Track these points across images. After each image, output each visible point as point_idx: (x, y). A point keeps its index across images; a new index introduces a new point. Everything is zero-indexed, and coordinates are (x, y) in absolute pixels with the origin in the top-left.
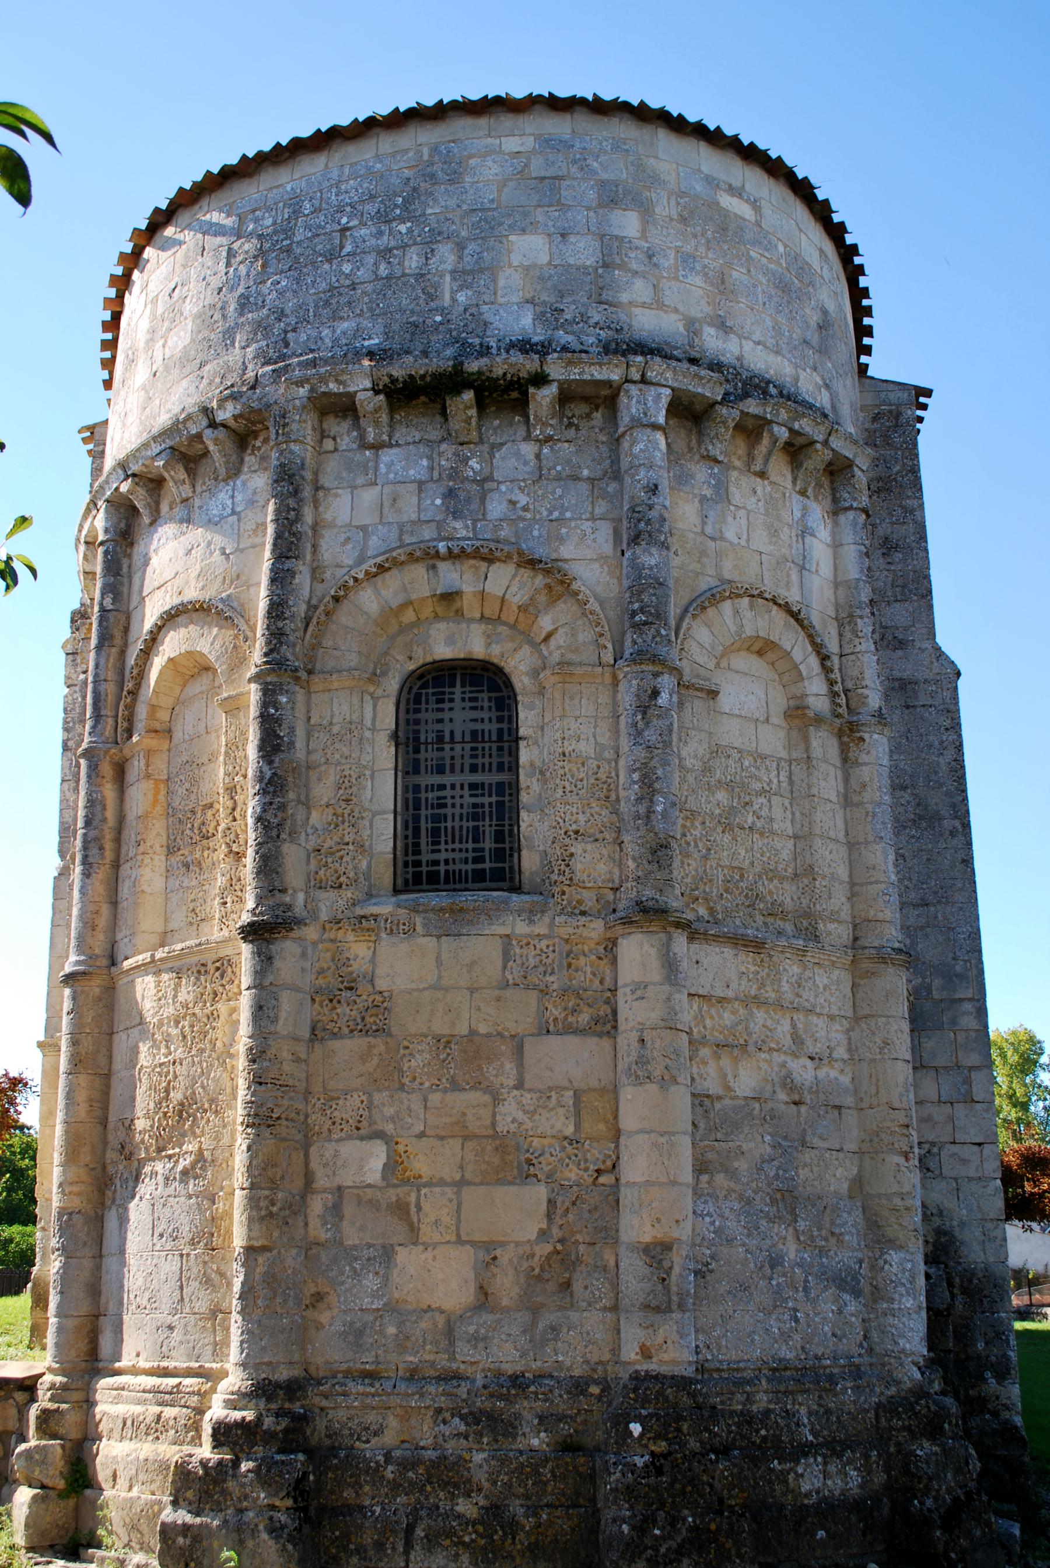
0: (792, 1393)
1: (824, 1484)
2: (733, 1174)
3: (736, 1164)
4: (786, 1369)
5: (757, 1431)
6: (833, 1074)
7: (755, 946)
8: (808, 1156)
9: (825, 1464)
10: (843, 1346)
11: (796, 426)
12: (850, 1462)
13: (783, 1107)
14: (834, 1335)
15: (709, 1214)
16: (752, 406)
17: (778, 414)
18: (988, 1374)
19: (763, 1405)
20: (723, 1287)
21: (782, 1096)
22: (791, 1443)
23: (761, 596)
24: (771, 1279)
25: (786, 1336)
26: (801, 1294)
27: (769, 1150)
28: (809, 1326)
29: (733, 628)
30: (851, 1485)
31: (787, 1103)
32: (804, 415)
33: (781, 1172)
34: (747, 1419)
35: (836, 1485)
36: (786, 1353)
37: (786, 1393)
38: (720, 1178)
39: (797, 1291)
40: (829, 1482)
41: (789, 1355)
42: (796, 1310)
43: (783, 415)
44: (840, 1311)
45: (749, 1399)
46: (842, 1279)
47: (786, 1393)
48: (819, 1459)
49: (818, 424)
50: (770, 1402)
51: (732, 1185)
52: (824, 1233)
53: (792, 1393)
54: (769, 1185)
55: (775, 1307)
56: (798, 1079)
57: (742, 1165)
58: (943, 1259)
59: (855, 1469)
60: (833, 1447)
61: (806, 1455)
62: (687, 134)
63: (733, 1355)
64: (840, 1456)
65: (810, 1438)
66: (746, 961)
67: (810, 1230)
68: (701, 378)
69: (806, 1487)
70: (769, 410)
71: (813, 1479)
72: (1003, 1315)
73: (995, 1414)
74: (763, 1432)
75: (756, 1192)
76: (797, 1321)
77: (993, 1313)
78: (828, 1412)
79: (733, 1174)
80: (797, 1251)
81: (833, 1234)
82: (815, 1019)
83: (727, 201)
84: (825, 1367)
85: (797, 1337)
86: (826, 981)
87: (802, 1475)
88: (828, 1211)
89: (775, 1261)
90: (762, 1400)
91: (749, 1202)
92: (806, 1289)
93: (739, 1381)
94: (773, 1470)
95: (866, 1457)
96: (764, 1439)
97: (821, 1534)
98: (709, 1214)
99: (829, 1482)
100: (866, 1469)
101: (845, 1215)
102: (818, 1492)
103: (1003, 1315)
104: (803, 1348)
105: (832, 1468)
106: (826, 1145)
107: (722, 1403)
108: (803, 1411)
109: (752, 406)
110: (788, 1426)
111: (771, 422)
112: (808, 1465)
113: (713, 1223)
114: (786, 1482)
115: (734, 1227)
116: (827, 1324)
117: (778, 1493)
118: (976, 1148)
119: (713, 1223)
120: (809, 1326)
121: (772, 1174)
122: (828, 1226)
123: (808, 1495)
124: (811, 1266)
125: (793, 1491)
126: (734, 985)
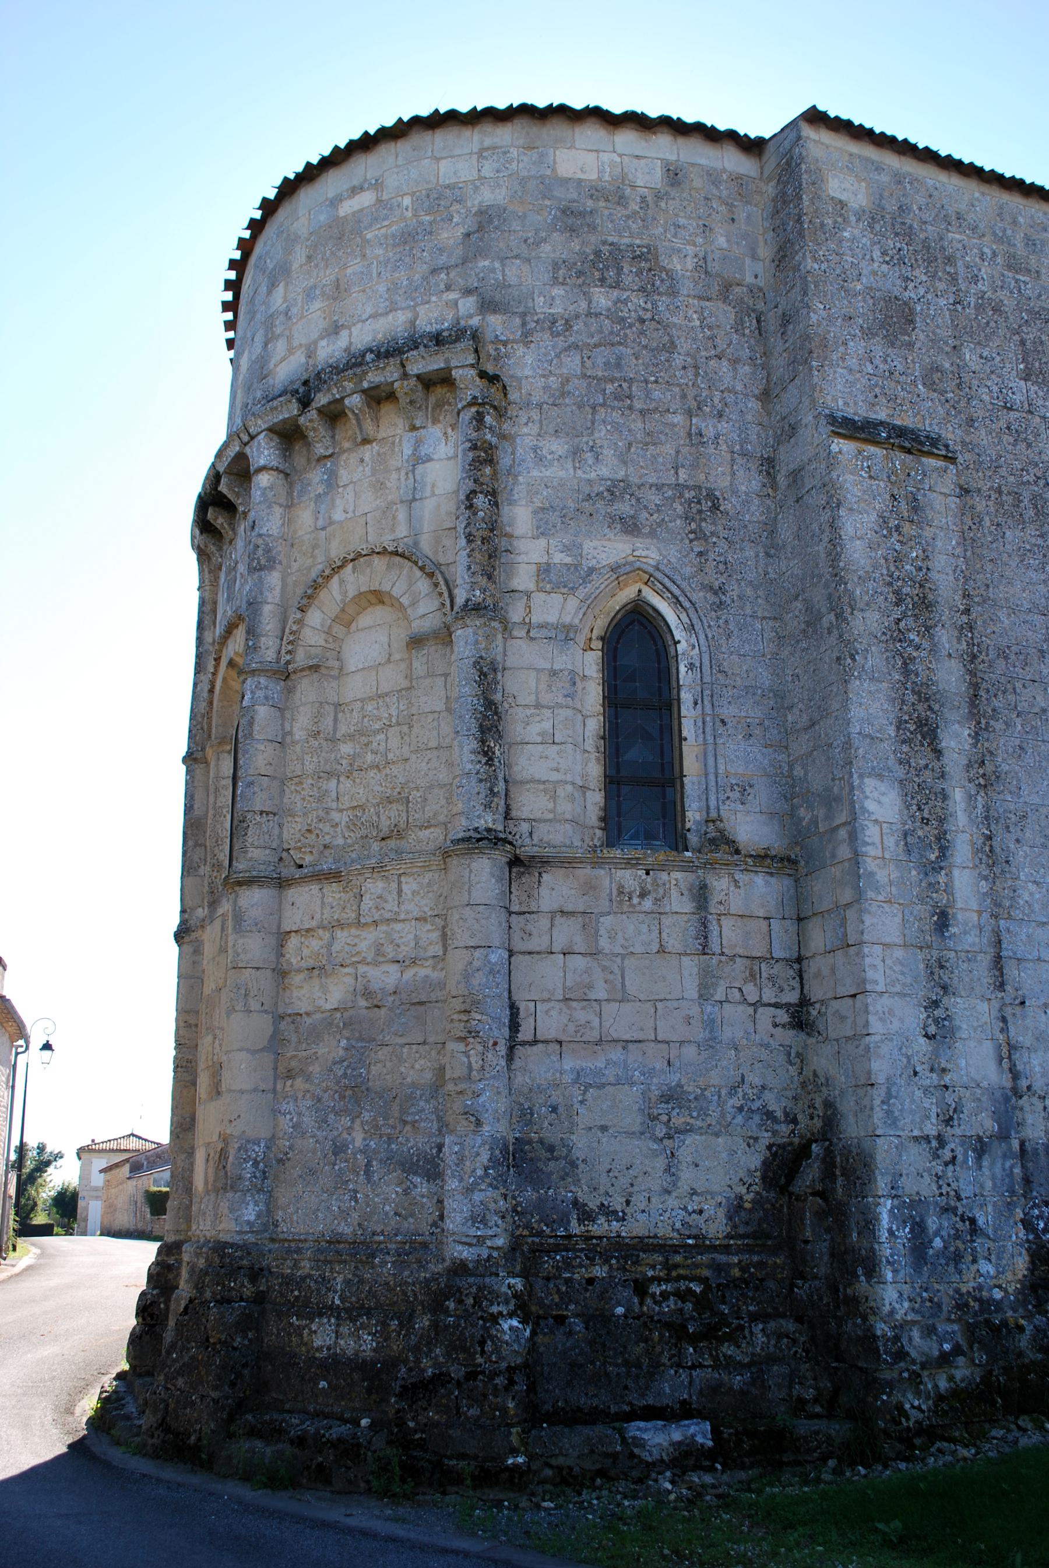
0: (330, 1262)
1: (336, 1343)
2: (308, 1078)
3: (311, 1069)
4: (339, 1242)
5: (292, 1291)
8: (382, 1053)
9: (338, 1325)
10: (409, 1224)
11: (365, 385)
12: (363, 1327)
13: (365, 1011)
14: (396, 1214)
15: (290, 1113)
16: (322, 399)
17: (344, 388)
19: (307, 1271)
20: (297, 1172)
21: (363, 1003)
22: (317, 1304)
23: (359, 555)
24: (334, 1164)
25: (345, 1214)
26: (362, 1178)
27: (341, 1052)
28: (368, 1205)
30: (364, 1347)
31: (367, 1008)
32: (365, 373)
33: (349, 1071)
34: (288, 1281)
35: (348, 1345)
36: (345, 1229)
37: (326, 1262)
38: (299, 1082)
39: (358, 1174)
40: (342, 1342)
41: (348, 1230)
42: (356, 1191)
43: (349, 386)
44: (406, 1192)
45: (296, 1266)
46: (412, 1163)
47: (326, 1262)
48: (333, 1320)
49: (384, 368)
50: (312, 1268)
52: (391, 1122)
53: (330, 1262)
54: (338, 1083)
55: (336, 1188)
56: (375, 986)
57: (315, 1069)
58: (829, 1135)
59: (369, 1334)
60: (352, 1313)
61: (321, 1315)
62: (319, 175)
63: (301, 1228)
64: (353, 1320)
65: (337, 1302)
66: (333, 892)
67: (375, 1119)
68: (276, 408)
69: (318, 1342)
70: (335, 391)
71: (322, 1336)
72: (871, 1200)
73: (865, 1319)
74: (296, 1293)
76: (357, 1201)
77: (863, 1197)
78: (361, 1281)
79: (308, 1078)
80: (364, 1139)
81: (405, 1123)
82: (398, 926)
84: (380, 1243)
85: (355, 1215)
86: (415, 887)
87: (315, 1332)
88: (398, 1101)
89: (339, 1149)
90: (306, 1266)
91: (319, 1100)
92: (368, 1173)
93: (292, 1248)
94: (292, 1324)
95: (385, 1324)
96: (297, 1297)
97: (323, 1384)
98: (290, 1113)
99: (342, 1342)
100: (384, 1335)
101: (422, 1103)
102: (329, 1349)
103: (871, 1200)
104: (359, 1225)
105: (344, 1330)
106: (403, 1040)
107: (277, 1266)
108: (340, 1279)
109: (322, 399)
110: (318, 1290)
111: (343, 398)
112: (321, 1325)
113: (291, 1120)
114: (301, 1335)
115: (309, 1121)
116: (384, 1203)
117: (294, 1344)
118: (850, 1001)
119: (291, 1120)
120: (368, 1205)
121: (340, 1073)
122: (397, 1115)
123: (319, 1349)
124: (376, 1152)
125: (306, 1344)
126: (318, 916)
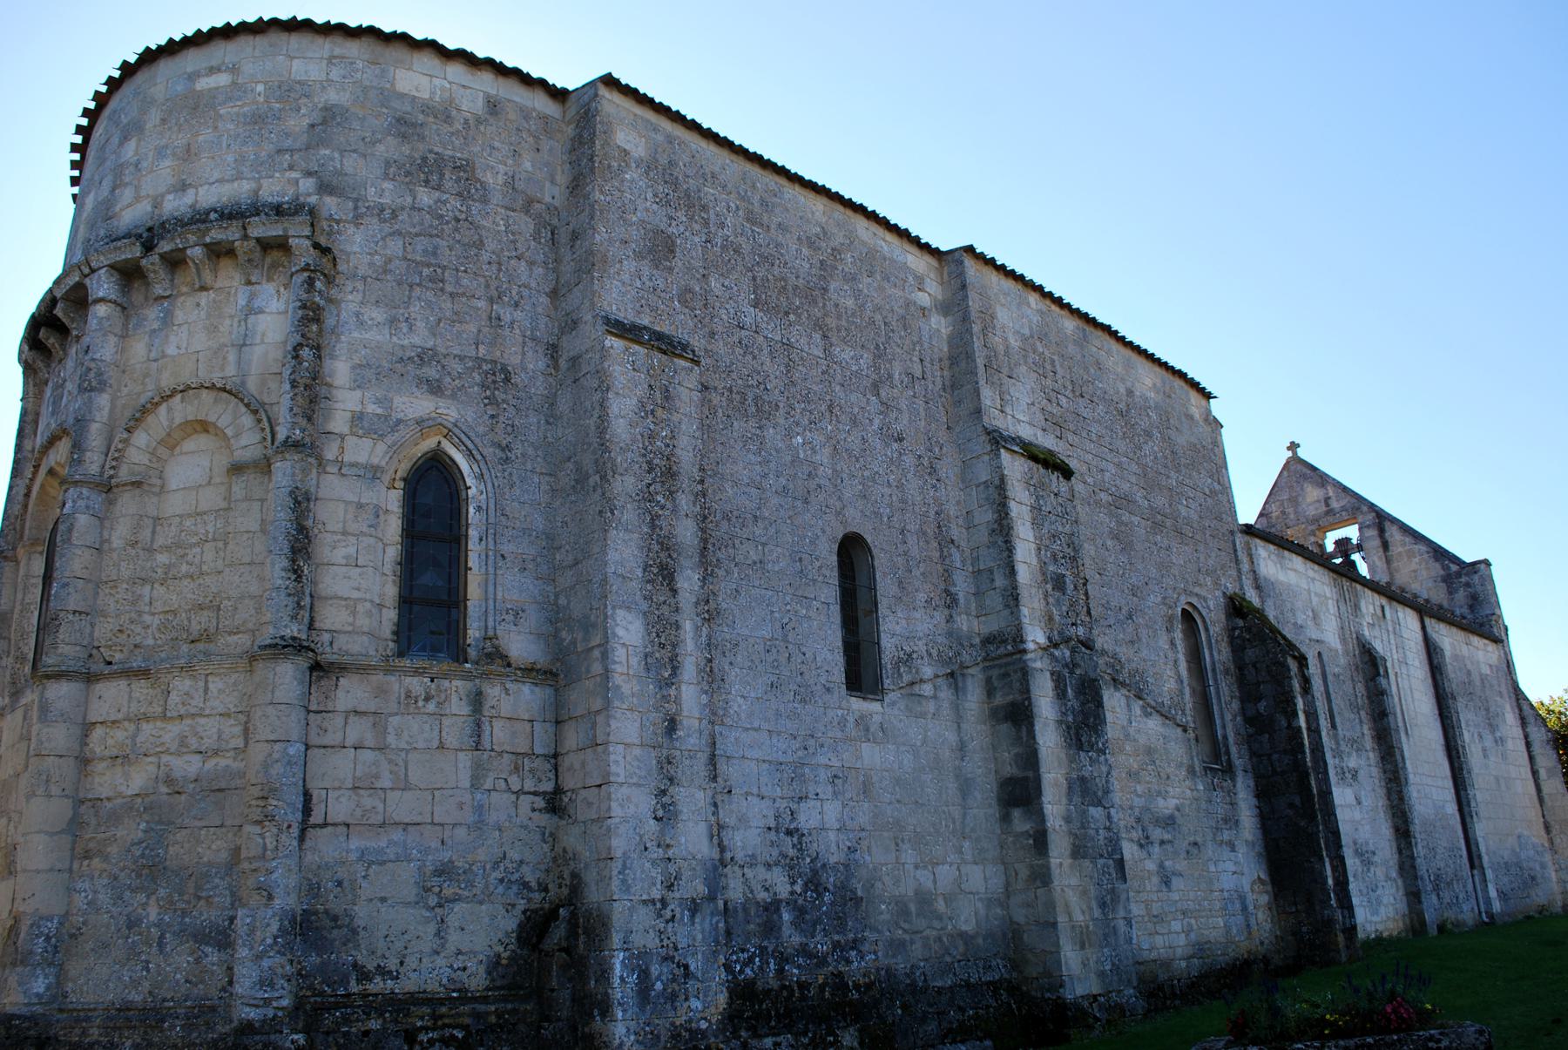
6: (229, 762)
7: (144, 673)
11: (208, 240)
16: (165, 246)
18: (596, 1012)
21: (164, 789)
25: (135, 983)
26: (155, 949)
27: (140, 834)
29: (166, 423)
32: (208, 230)
36: (136, 997)
37: (115, 1028)
38: (96, 861)
41: (138, 998)
42: (148, 962)
43: (192, 238)
44: (198, 961)
45: (84, 1033)
51: (104, 866)
56: (177, 774)
57: (113, 850)
63: (91, 998)
66: (141, 688)
75: (122, 870)
83: (203, 84)
85: (146, 984)
92: (161, 945)
109: (165, 246)
118: (596, 790)
